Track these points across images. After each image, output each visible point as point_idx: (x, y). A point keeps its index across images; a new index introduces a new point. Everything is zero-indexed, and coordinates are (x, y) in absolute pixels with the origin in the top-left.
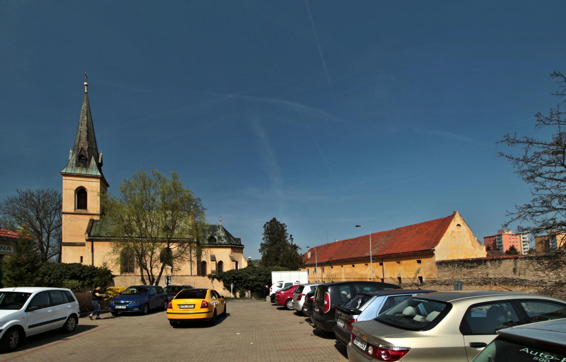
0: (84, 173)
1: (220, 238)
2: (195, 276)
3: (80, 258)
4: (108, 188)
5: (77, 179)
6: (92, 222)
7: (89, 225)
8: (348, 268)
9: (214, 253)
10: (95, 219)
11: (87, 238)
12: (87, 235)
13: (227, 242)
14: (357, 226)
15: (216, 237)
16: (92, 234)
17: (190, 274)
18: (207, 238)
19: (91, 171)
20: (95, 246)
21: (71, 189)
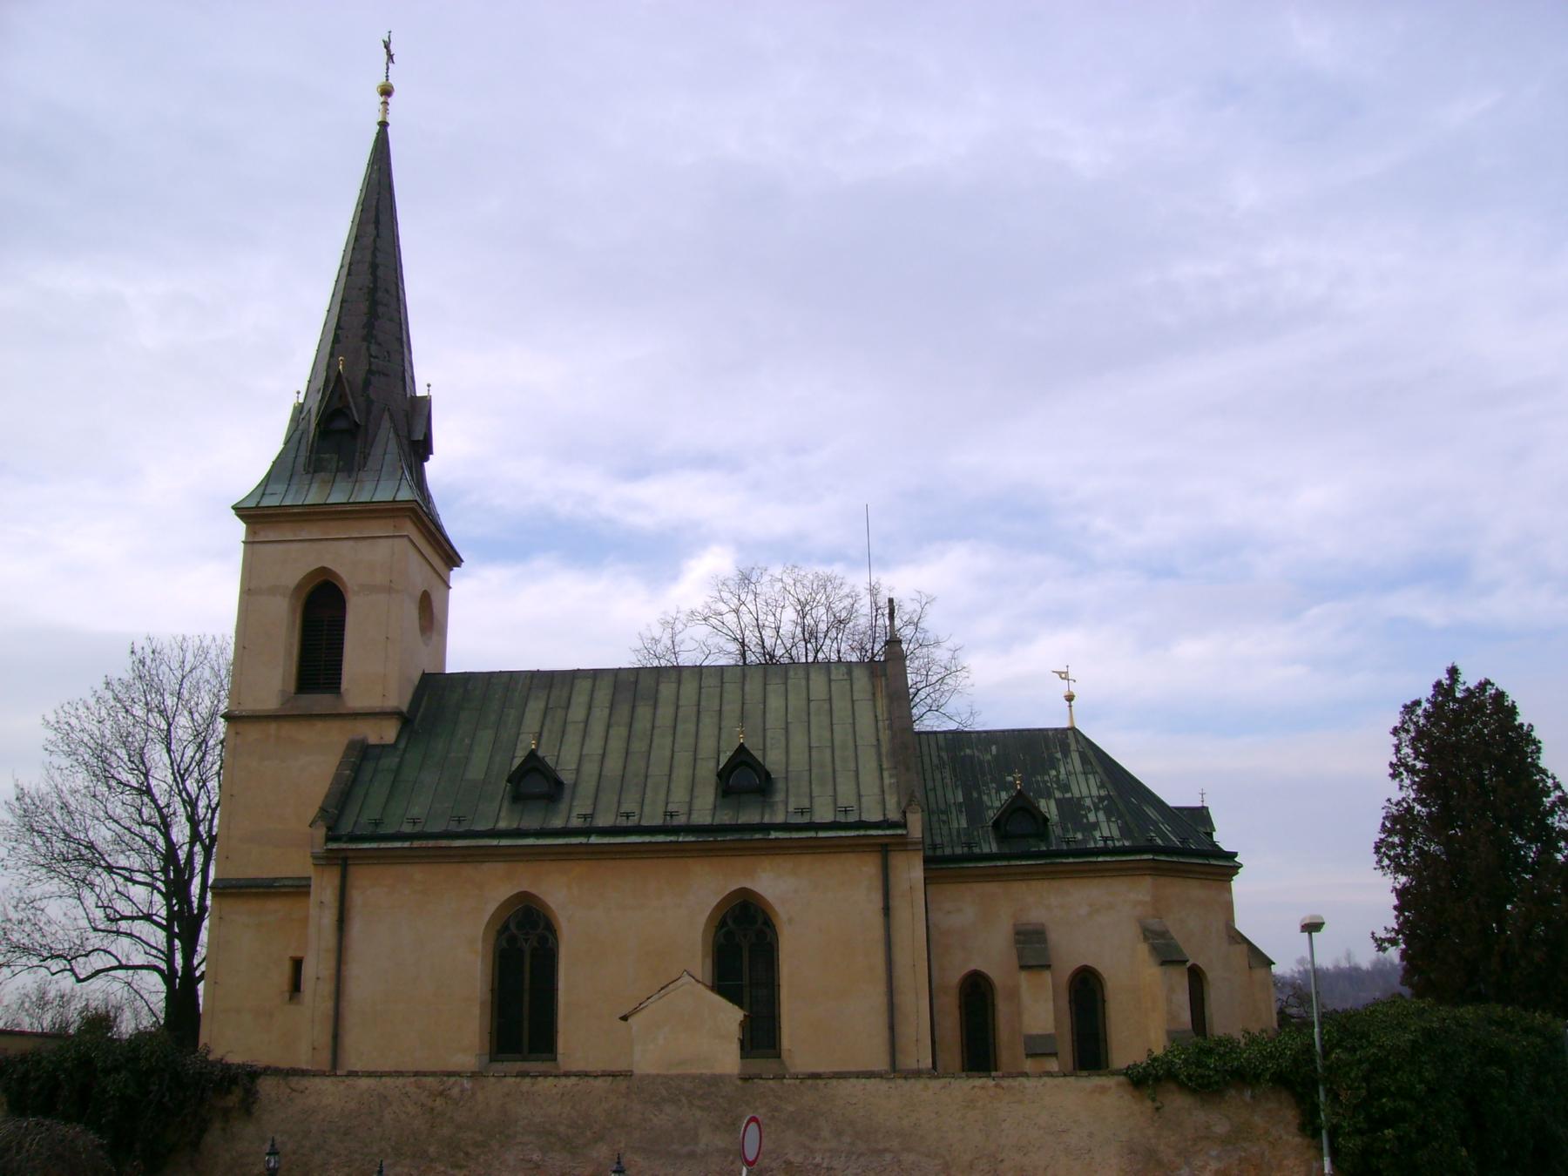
0: (338, 497)
1: (1072, 809)
2: (917, 1074)
3: (287, 968)
4: (455, 576)
5: (313, 531)
6: (361, 756)
7: (337, 777)
8: (743, 819)
9: (1036, 915)
10: (373, 739)
11: (320, 848)
12: (321, 832)
13: (1125, 832)
14: (625, 1018)
15: (1048, 808)
16: (346, 827)
17: (882, 1064)
18: (991, 814)
19: (369, 486)
20: (356, 897)
21: (273, 591)
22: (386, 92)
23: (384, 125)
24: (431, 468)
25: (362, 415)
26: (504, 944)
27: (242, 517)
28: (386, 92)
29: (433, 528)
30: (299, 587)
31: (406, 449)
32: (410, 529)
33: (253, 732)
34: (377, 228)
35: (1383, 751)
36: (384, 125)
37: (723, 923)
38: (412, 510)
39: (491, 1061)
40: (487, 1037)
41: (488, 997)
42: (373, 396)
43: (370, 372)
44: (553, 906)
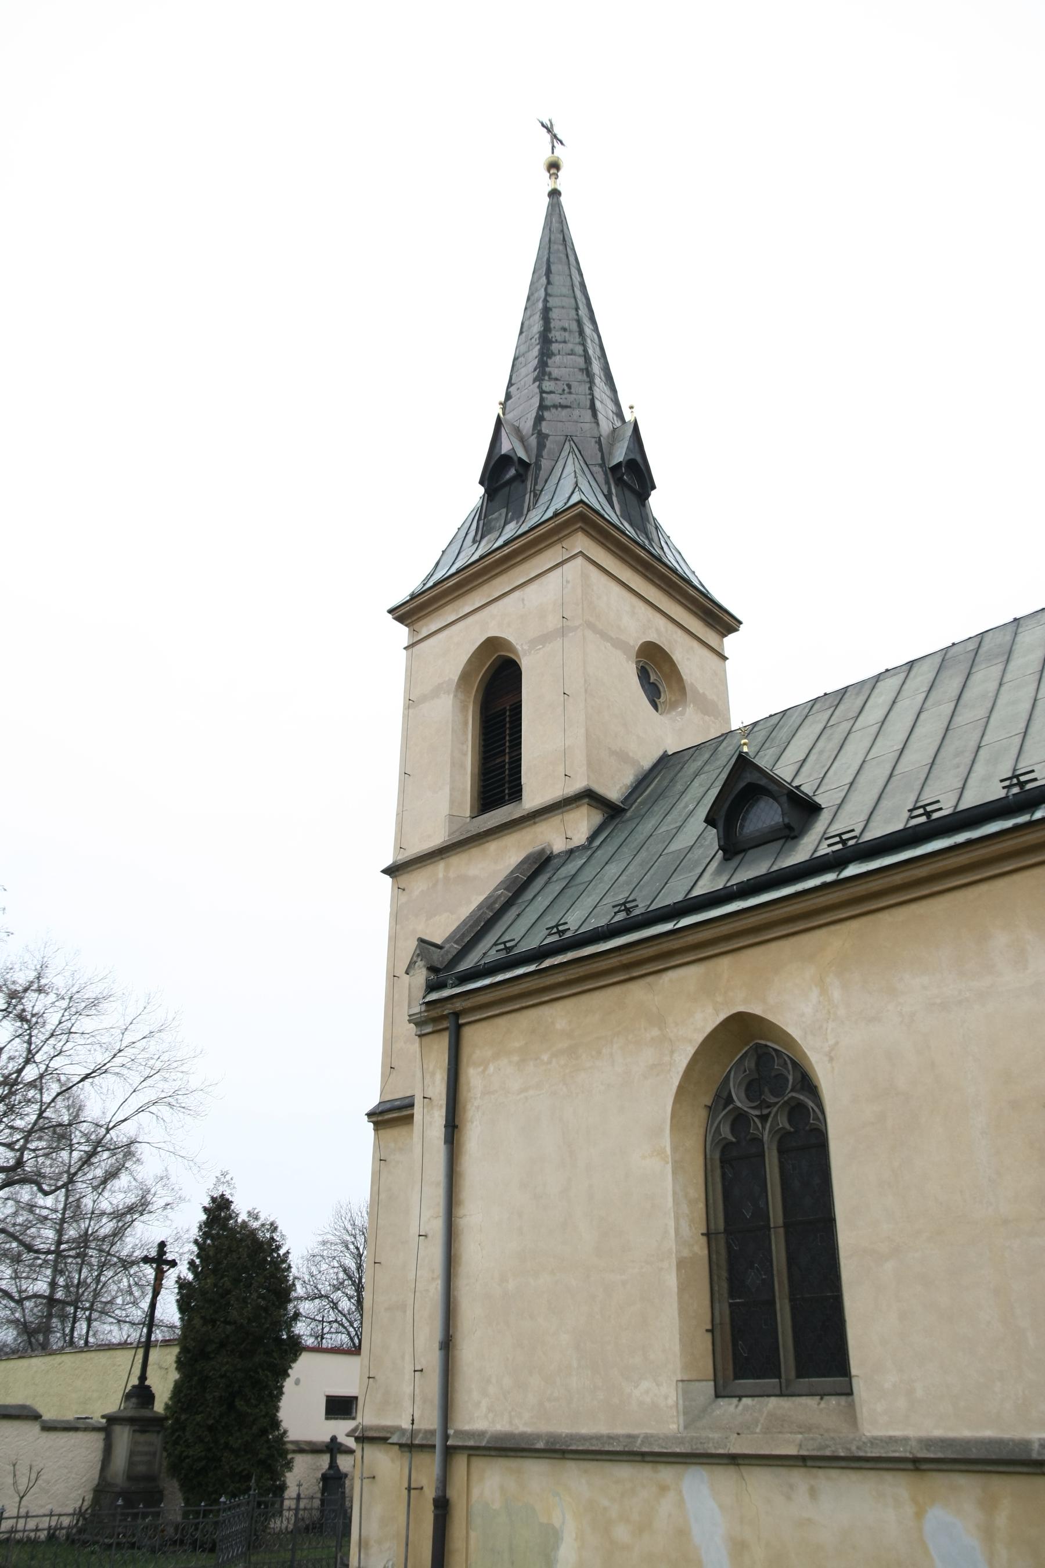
12: (421, 976)
20: (473, 1078)
22: (554, 166)
23: (555, 194)
24: (656, 502)
25: (565, 476)
26: (726, 1132)
27: (400, 619)
28: (554, 166)
29: (709, 605)
30: (465, 677)
31: (601, 478)
32: (581, 542)
33: (418, 881)
34: (548, 278)
35: (266, 1216)
36: (555, 194)
37: (722, 1099)
38: (581, 517)
39: (718, 1396)
40: (704, 1343)
41: (700, 1248)
42: (545, 430)
43: (542, 407)
44: (794, 1032)
